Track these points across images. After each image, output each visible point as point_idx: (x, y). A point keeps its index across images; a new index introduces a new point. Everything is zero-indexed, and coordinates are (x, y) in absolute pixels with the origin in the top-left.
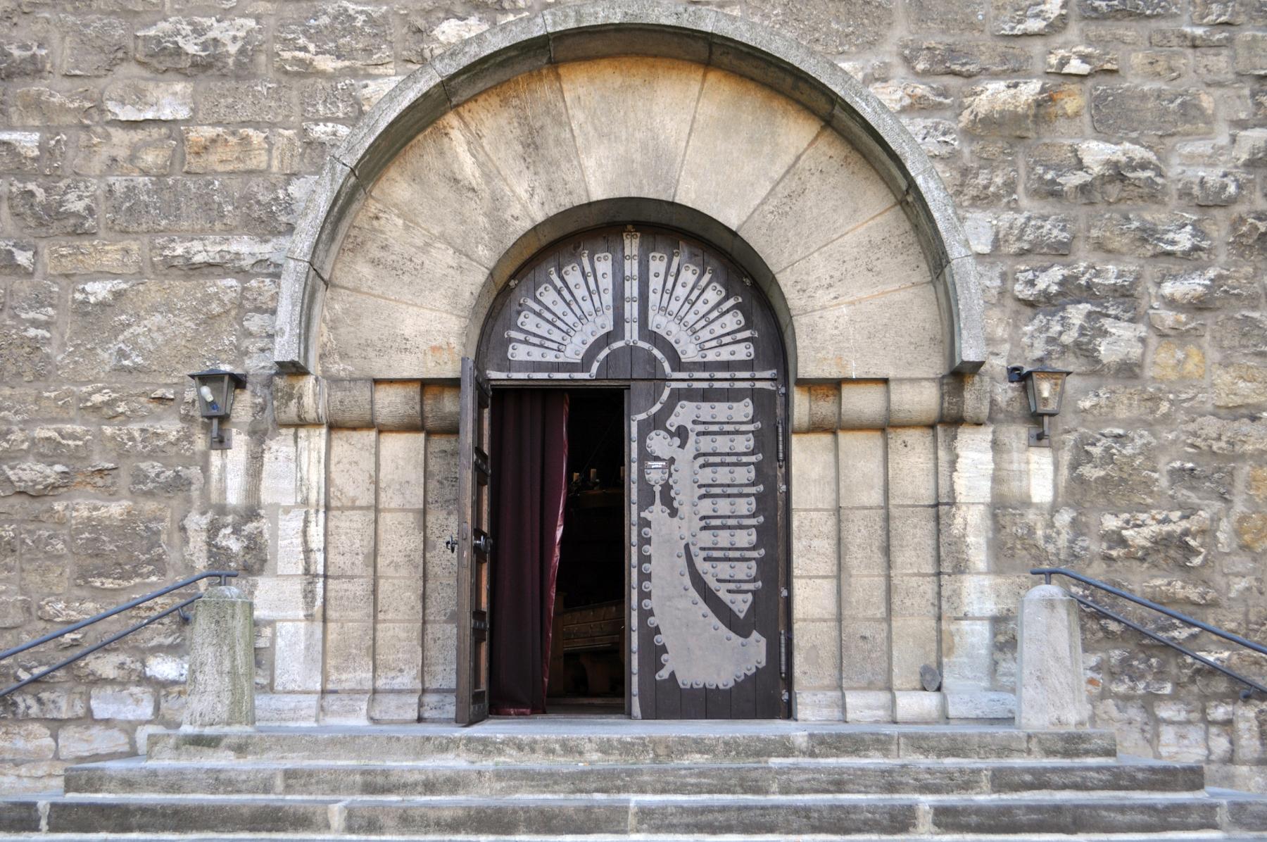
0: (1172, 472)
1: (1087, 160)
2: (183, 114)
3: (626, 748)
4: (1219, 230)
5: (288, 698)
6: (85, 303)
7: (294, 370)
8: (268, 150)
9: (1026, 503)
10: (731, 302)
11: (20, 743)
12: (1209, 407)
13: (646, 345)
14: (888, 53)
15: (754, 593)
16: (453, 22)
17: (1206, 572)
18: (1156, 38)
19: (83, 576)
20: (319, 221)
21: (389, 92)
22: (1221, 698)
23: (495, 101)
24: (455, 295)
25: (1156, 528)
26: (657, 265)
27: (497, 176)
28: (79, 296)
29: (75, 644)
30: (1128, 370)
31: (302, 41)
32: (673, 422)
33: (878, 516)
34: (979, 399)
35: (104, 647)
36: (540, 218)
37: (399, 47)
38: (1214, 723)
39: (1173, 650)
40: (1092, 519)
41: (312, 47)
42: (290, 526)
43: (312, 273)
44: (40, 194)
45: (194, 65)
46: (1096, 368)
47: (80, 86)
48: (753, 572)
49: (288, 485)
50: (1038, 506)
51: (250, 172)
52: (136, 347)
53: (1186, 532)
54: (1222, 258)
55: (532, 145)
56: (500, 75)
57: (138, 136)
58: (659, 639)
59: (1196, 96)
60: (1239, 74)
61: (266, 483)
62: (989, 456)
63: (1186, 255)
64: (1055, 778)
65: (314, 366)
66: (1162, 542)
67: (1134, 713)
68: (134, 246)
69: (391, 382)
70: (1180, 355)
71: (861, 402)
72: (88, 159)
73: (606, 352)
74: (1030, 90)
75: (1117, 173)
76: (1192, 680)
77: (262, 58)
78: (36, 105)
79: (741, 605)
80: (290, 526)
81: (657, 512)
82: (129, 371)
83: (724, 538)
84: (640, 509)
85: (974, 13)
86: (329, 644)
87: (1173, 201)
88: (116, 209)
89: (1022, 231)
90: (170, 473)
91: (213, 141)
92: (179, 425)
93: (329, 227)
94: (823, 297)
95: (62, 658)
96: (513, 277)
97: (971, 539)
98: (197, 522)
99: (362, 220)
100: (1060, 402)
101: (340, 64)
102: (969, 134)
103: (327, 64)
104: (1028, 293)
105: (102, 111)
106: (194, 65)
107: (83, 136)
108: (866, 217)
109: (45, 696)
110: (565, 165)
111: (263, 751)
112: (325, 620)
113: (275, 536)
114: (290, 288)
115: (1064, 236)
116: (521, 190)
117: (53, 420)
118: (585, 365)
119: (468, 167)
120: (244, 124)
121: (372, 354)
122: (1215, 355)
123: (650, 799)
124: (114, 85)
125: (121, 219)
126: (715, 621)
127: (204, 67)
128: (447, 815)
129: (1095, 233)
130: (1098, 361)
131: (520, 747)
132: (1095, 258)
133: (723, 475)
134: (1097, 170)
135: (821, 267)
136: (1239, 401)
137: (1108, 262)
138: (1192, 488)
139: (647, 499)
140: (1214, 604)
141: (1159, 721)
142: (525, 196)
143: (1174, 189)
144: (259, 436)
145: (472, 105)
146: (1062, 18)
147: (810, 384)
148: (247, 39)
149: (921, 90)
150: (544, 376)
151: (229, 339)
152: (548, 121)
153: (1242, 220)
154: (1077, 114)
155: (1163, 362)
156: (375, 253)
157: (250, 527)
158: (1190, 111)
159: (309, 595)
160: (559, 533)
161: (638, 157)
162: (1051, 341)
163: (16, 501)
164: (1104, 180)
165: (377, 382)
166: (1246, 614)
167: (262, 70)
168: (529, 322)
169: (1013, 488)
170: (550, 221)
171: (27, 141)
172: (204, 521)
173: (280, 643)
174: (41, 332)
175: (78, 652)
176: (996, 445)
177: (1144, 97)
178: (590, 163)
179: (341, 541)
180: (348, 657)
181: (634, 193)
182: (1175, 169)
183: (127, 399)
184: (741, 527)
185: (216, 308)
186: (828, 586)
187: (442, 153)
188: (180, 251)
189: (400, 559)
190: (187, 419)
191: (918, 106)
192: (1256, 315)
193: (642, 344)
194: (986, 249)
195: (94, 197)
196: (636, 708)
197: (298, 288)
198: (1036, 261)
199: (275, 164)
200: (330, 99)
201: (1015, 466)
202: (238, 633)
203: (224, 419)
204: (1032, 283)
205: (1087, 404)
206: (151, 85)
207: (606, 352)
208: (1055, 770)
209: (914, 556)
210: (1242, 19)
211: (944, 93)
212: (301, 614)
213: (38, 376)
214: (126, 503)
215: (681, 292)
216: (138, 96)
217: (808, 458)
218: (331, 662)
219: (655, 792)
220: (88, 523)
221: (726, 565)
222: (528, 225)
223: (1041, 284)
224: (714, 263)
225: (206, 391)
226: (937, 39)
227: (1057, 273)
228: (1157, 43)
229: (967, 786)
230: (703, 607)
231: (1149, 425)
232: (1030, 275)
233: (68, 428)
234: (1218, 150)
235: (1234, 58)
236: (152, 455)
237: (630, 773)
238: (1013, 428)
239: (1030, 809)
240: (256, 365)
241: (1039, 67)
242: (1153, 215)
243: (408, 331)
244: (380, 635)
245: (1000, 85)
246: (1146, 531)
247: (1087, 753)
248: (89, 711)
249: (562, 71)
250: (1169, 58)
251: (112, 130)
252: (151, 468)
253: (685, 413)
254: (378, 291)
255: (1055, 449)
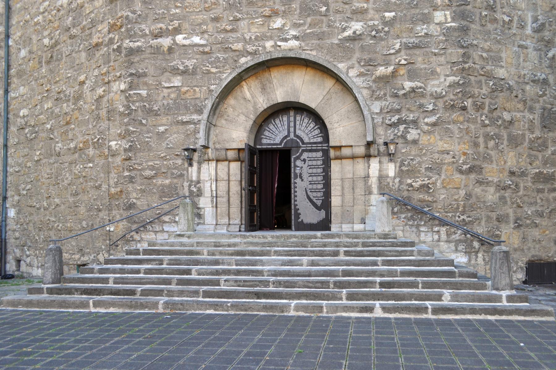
0: (426, 168)
1: (405, 87)
2: (180, 84)
3: (278, 237)
4: (440, 104)
5: (207, 226)
6: (159, 132)
7: (206, 147)
8: (200, 93)
9: (388, 176)
10: (317, 127)
11: (148, 237)
12: (436, 151)
13: (295, 138)
14: (354, 61)
15: (322, 200)
16: (244, 58)
17: (434, 193)
18: (425, 53)
19: (160, 198)
20: (209, 111)
21: (227, 77)
22: (437, 225)
23: (254, 78)
24: (245, 127)
25: (421, 182)
26: (298, 118)
27: (256, 97)
28: (157, 130)
29: (159, 213)
30: (415, 142)
31: (208, 65)
32: (302, 158)
33: (351, 180)
34: (374, 150)
35: (165, 214)
36: (266, 107)
37: (231, 65)
38: (435, 232)
39: (425, 213)
40: (404, 180)
41: (210, 66)
42: (208, 185)
43: (208, 123)
44: (147, 106)
45: (182, 72)
46: (406, 142)
47: (156, 79)
48: (322, 195)
49: (207, 175)
50: (390, 177)
51: (196, 98)
52: (171, 142)
53: (429, 183)
54: (441, 112)
55: (264, 89)
56: (254, 71)
57: (170, 90)
58: (299, 211)
59: (435, 68)
60: (447, 62)
61: (202, 175)
62: (378, 165)
63: (431, 111)
64: (378, 244)
65: (211, 145)
66: (422, 186)
67: (414, 229)
68: (170, 118)
69: (231, 149)
70: (429, 138)
71: (346, 152)
72: (158, 96)
73: (286, 140)
74: (391, 69)
75: (413, 90)
76: (429, 221)
77: (198, 69)
78: (146, 84)
79: (319, 203)
80: (208, 185)
81: (298, 180)
82: (170, 148)
83: (315, 186)
84: (294, 179)
85: (377, 49)
86: (218, 213)
87: (428, 97)
88: (165, 109)
89: (388, 106)
90: (179, 173)
91: (187, 91)
92: (181, 161)
93: (212, 112)
94: (336, 125)
95: (157, 217)
96: (263, 122)
97: (373, 186)
98: (186, 184)
99: (223, 109)
100: (395, 151)
101: (217, 70)
102: (374, 81)
103: (214, 70)
104: (389, 122)
105: (161, 85)
106: (182, 72)
107: (157, 91)
108: (347, 105)
109: (153, 226)
110: (271, 94)
111: (194, 238)
112: (216, 207)
113: (204, 187)
114: (202, 127)
115: (399, 107)
116: (261, 100)
117: (152, 161)
118: (280, 144)
119: (248, 95)
120: (194, 86)
121: (225, 143)
122: (438, 137)
123: (276, 249)
124: (163, 78)
125: (166, 111)
126: (312, 207)
127: (184, 72)
128: (230, 252)
129: (407, 106)
130: (407, 140)
131: (253, 237)
132: (407, 113)
133: (314, 171)
134: (408, 89)
135: (335, 118)
136: (444, 149)
137: (410, 114)
138: (431, 172)
139: (296, 177)
140: (435, 202)
141: (420, 231)
142: (262, 102)
143: (429, 94)
144: (200, 163)
145: (249, 79)
146: (400, 49)
147: (335, 148)
148: (194, 65)
149: (362, 70)
150: (270, 147)
151: (192, 140)
152: (267, 82)
153: (447, 101)
154: (403, 75)
155: (424, 139)
156: (226, 118)
157: (198, 185)
158: (434, 73)
159: (212, 201)
160: (276, 186)
161: (290, 91)
162: (395, 135)
163: (145, 180)
164: (410, 92)
165: (227, 149)
166: (444, 204)
167: (198, 72)
168: (266, 133)
169: (384, 173)
170: (268, 108)
171: (144, 93)
172: (188, 184)
173: (206, 213)
174: (149, 139)
175: (160, 215)
176: (380, 162)
177: (421, 69)
178: (278, 93)
179: (220, 188)
180: (223, 216)
181: (289, 100)
182: (429, 88)
183: (169, 155)
184: (319, 184)
185: (189, 132)
186: (340, 198)
187: (242, 92)
188: (180, 119)
189: (235, 192)
190: (183, 159)
191: (361, 75)
192: (449, 126)
193: (294, 138)
194: (379, 111)
195: (160, 106)
196: (293, 228)
197: (204, 127)
198: (392, 114)
199: (202, 96)
200: (215, 79)
201: (385, 167)
202: (189, 210)
203: (191, 159)
204: (390, 120)
205: (404, 151)
206: (172, 78)
207: (286, 140)
208: (377, 242)
209: (360, 190)
210: (449, 47)
211: (368, 71)
212: (211, 206)
213: (149, 150)
214: (170, 180)
215: (304, 125)
216: (169, 81)
217: (335, 166)
218: (219, 217)
219: (281, 247)
220: (161, 185)
221: (315, 193)
222: (263, 109)
223: (393, 120)
224: (312, 117)
225: (186, 153)
226: (366, 57)
227: (397, 117)
228: (426, 54)
229: (356, 246)
230: (310, 204)
231: (420, 156)
232: (390, 118)
233: (156, 162)
234: (441, 83)
235: (446, 58)
236: (175, 169)
237: (275, 243)
238: (385, 157)
239: (367, 251)
240: (198, 146)
241: (393, 63)
242: (423, 101)
243: (234, 137)
244: (231, 211)
245: (383, 68)
246: (418, 183)
247: (389, 238)
248: (163, 229)
249: (271, 69)
250: (428, 58)
251: (163, 89)
252: (175, 171)
253: (305, 155)
254: (227, 127)
255: (395, 162)
